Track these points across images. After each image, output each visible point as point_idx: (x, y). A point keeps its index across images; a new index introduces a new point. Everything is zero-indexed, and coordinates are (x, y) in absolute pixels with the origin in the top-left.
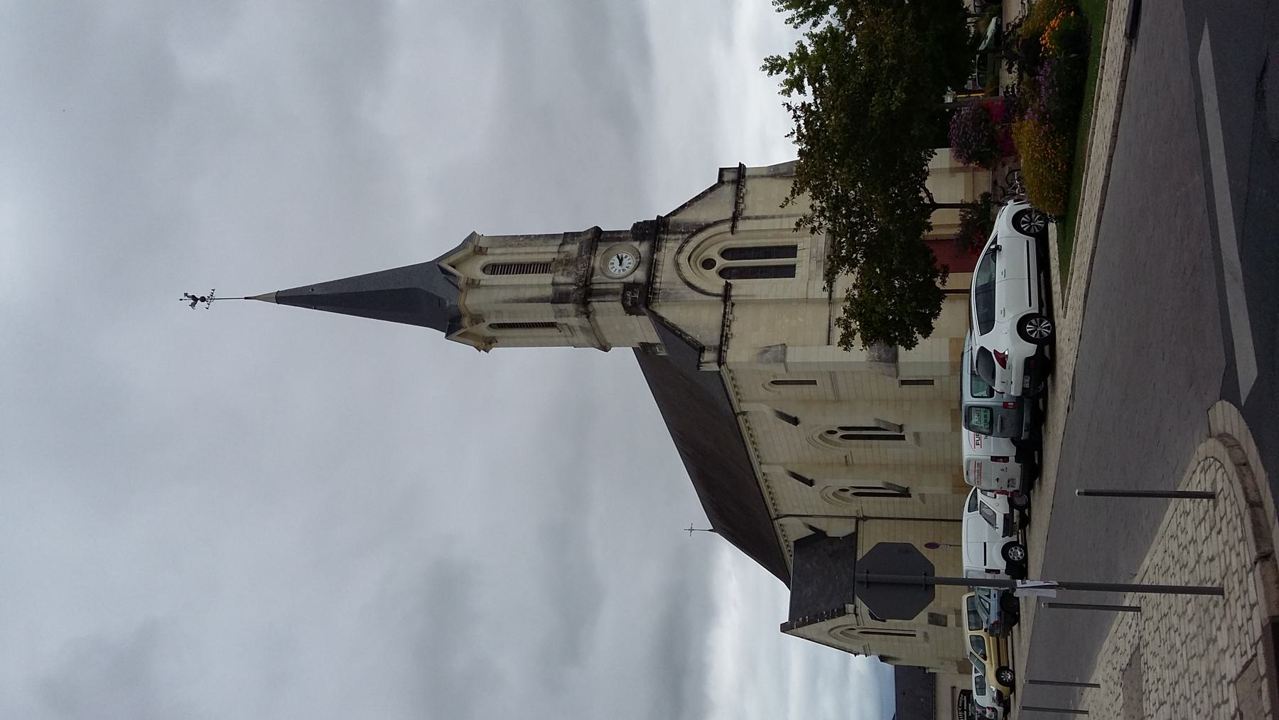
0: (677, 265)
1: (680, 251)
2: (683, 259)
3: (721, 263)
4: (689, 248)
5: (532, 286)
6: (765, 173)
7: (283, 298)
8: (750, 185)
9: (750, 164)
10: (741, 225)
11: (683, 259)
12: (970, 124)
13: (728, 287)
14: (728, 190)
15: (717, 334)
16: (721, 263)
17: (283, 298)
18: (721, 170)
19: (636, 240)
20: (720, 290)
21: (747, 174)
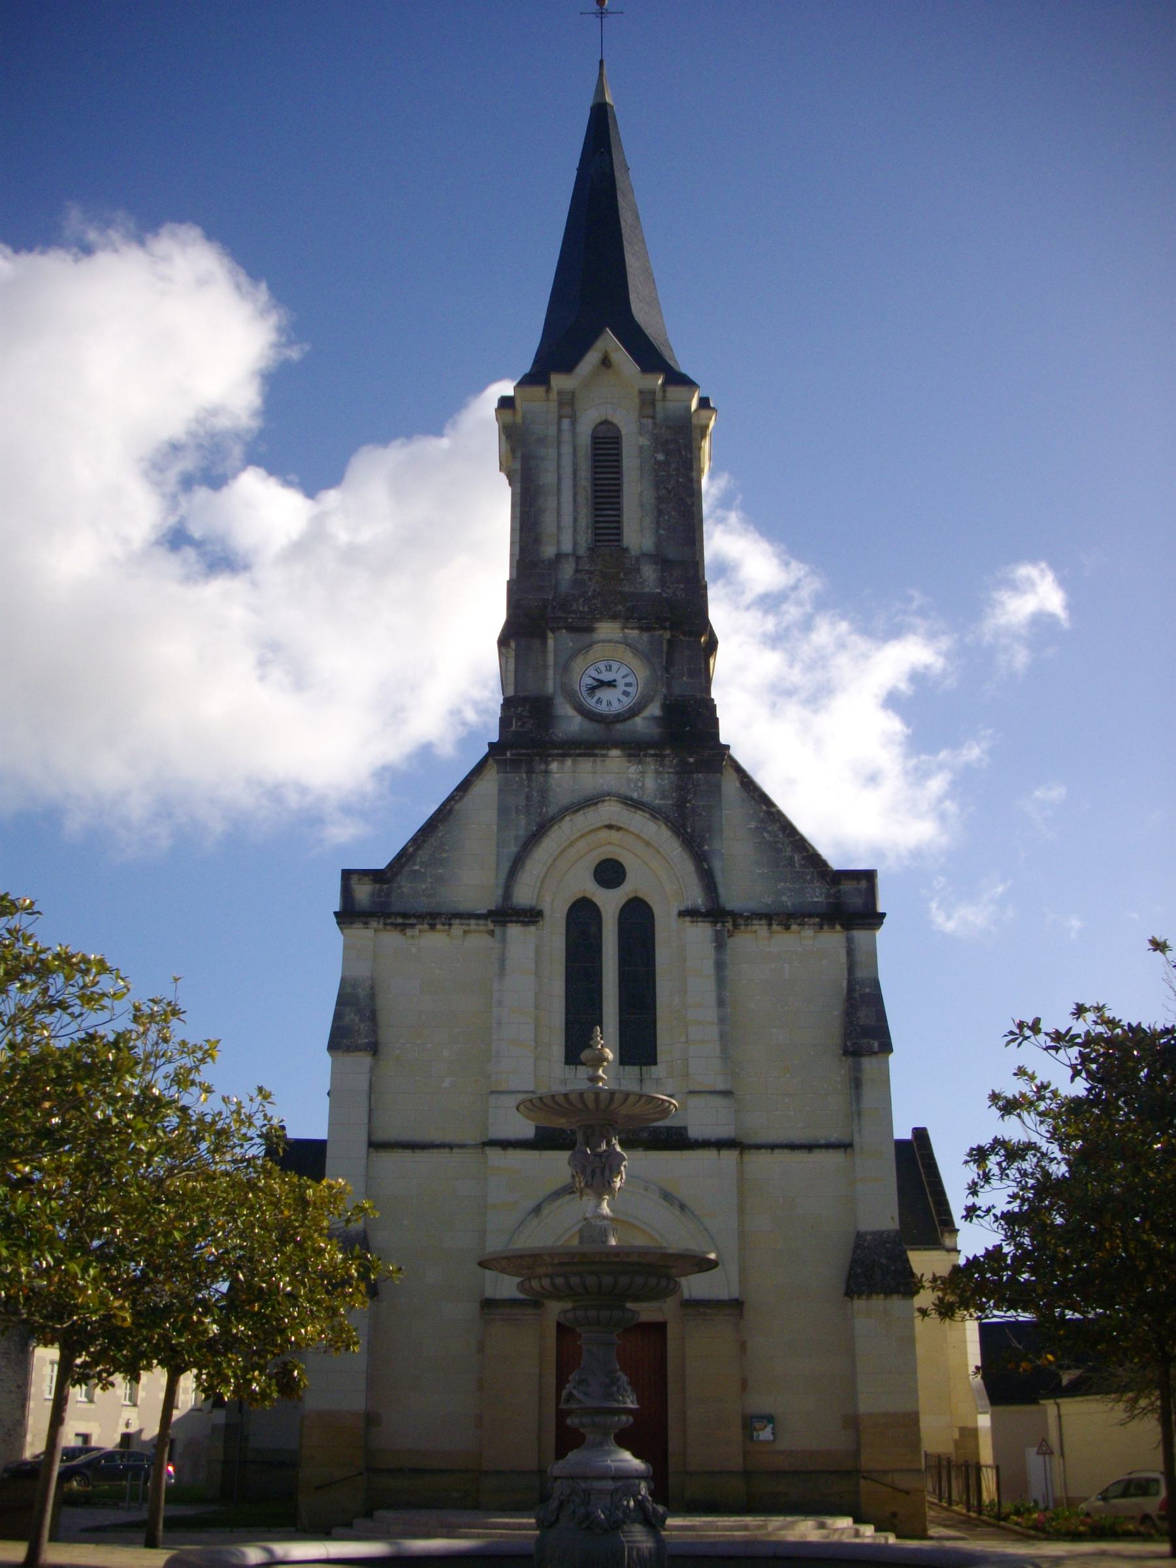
0: (592, 801)
1: (635, 804)
2: (610, 811)
3: (610, 903)
4: (639, 821)
5: (575, 511)
6: (860, 974)
7: (601, 122)
8: (833, 940)
9: (883, 936)
10: (700, 934)
11: (610, 811)
12: (35, 1050)
13: (531, 916)
14: (817, 895)
15: (422, 904)
16: (610, 903)
17: (601, 122)
18: (347, 875)
19: (665, 707)
20: (523, 896)
21: (859, 935)
